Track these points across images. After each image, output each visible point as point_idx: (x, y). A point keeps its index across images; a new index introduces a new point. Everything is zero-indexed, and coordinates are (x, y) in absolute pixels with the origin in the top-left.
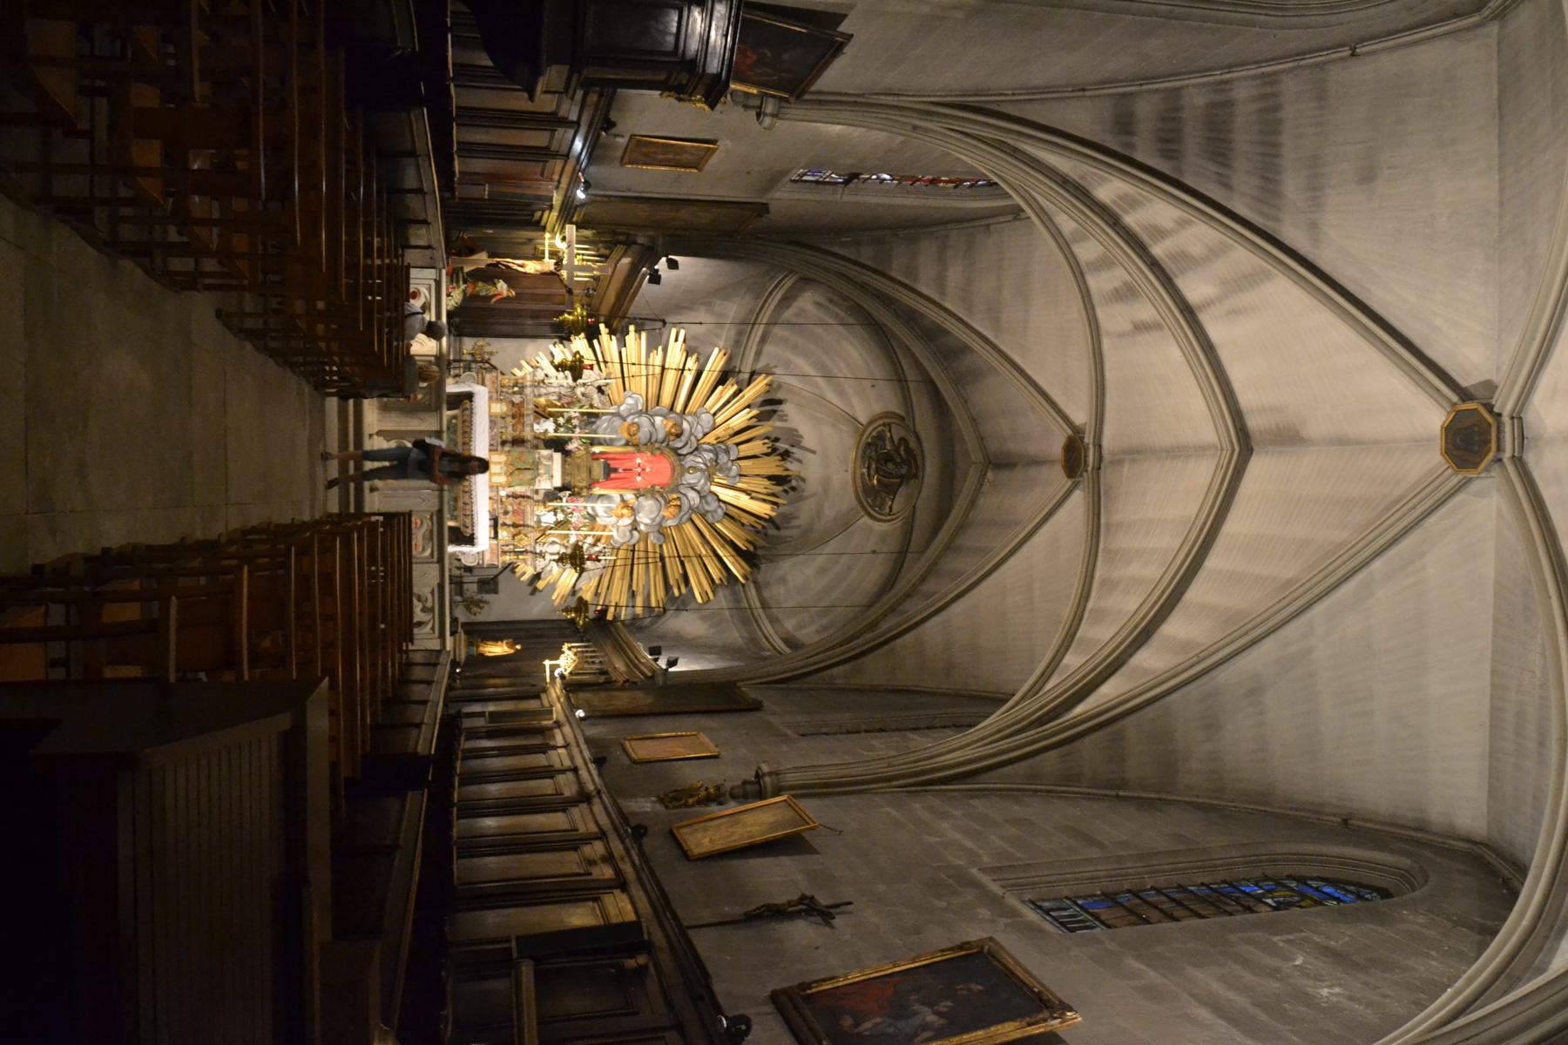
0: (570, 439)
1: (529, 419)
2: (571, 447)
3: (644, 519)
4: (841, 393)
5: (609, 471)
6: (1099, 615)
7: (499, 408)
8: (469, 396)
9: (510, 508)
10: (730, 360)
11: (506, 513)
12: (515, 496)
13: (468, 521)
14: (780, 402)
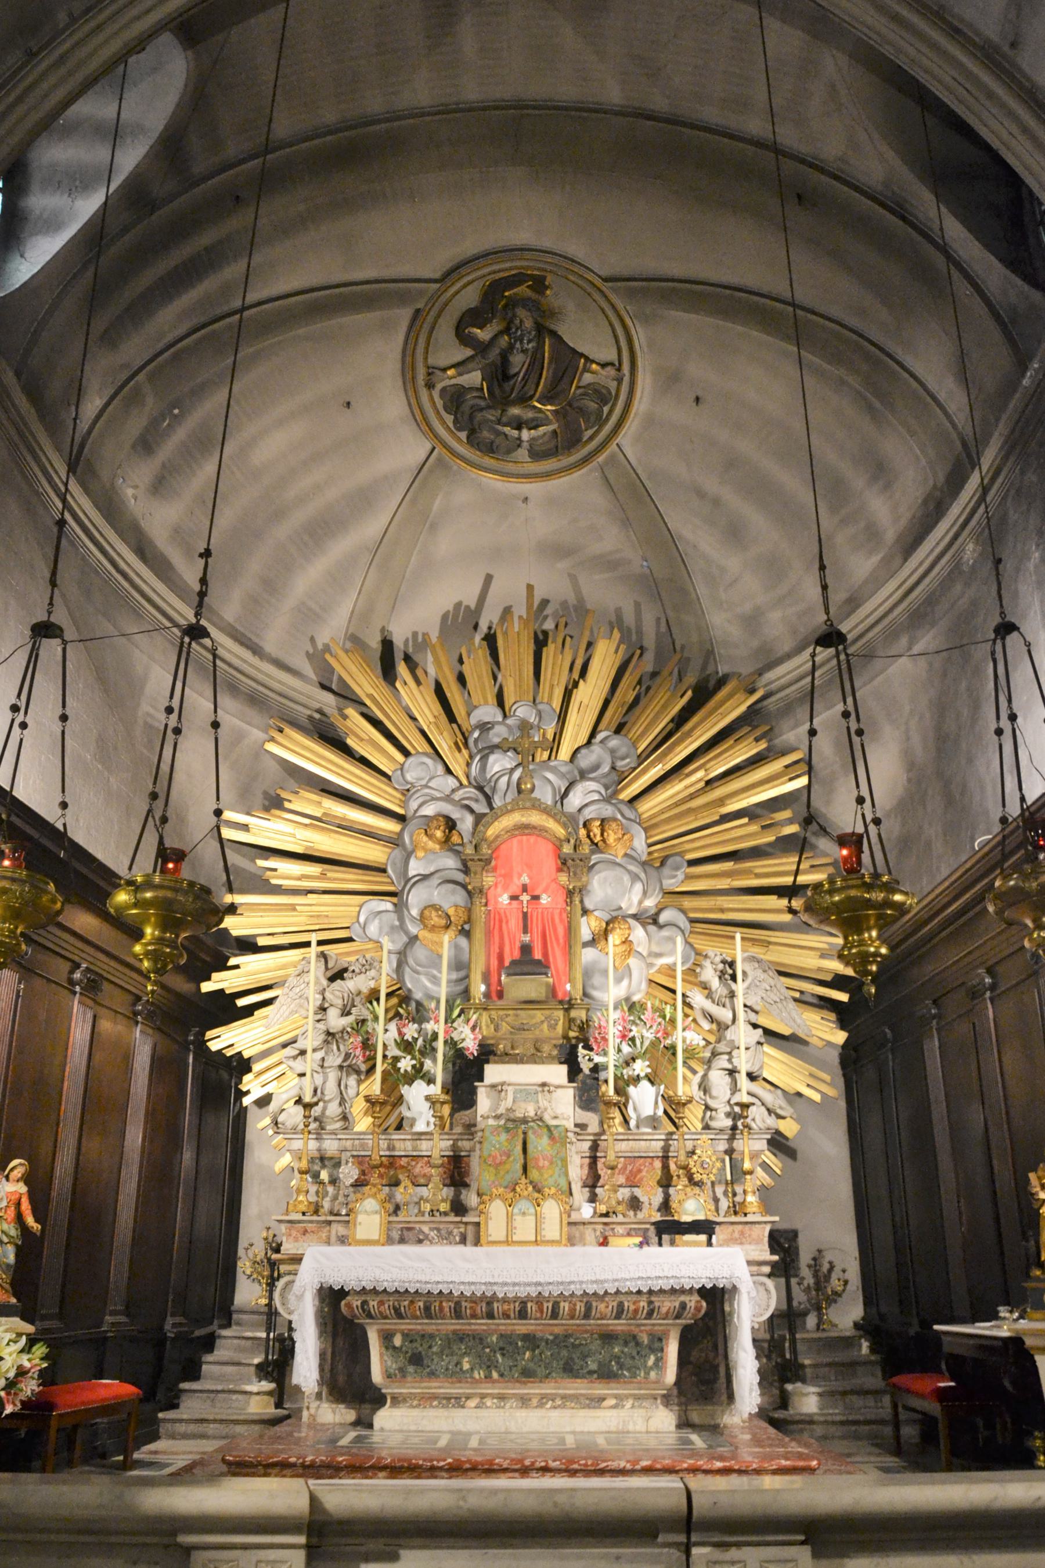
0: (450, 1043)
1: (403, 1145)
2: (470, 1044)
3: (634, 898)
4: (363, 500)
5: (527, 963)
6: (595, 836)
7: (369, 1215)
8: (332, 1298)
9: (624, 1193)
10: (295, 724)
11: (635, 1204)
12: (593, 1182)
13: (668, 1304)
14: (387, 645)
